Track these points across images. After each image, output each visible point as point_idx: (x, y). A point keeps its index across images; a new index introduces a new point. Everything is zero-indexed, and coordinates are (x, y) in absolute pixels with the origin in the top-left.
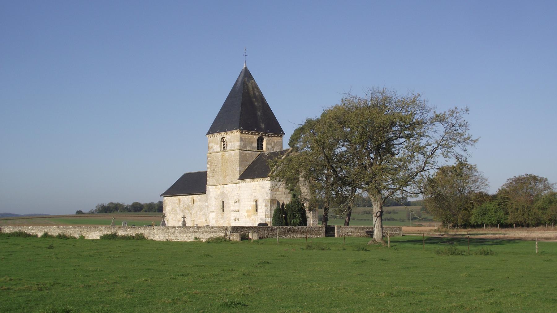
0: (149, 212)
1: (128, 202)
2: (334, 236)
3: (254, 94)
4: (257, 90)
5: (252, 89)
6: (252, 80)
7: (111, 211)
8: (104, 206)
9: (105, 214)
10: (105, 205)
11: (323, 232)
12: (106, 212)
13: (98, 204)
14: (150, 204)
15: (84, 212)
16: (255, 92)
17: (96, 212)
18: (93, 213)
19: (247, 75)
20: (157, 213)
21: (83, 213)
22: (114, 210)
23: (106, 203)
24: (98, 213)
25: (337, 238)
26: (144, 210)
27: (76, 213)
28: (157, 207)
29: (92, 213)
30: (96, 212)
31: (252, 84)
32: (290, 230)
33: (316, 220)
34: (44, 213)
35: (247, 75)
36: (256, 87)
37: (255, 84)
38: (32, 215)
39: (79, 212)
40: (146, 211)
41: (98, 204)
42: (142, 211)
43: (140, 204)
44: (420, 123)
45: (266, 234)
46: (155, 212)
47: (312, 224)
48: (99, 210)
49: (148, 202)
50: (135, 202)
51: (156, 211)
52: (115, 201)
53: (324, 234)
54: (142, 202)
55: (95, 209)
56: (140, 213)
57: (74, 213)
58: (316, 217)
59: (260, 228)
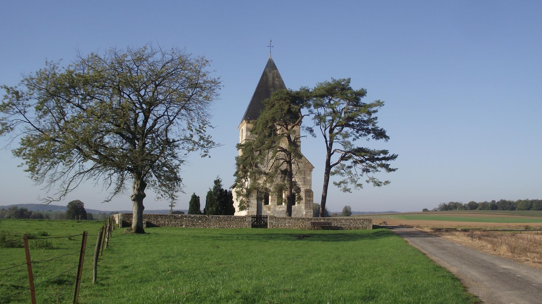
0: (483, 210)
1: (465, 201)
2: (267, 228)
3: (273, 83)
4: (278, 79)
5: (271, 79)
6: (275, 70)
7: (451, 209)
8: (445, 204)
9: (447, 212)
10: (446, 204)
11: (248, 222)
12: (447, 210)
13: (441, 204)
14: (484, 203)
15: (429, 210)
16: (275, 82)
17: (438, 210)
18: (436, 210)
19: (271, 66)
20: (490, 211)
21: (428, 211)
22: (453, 208)
23: (447, 203)
24: (440, 210)
25: (269, 229)
26: (479, 208)
27: (67, 205)
28: (490, 206)
29: (435, 210)
30: (438, 210)
31: (273, 74)
32: (200, 219)
33: (310, 211)
34: (28, 203)
35: (271, 66)
36: (279, 76)
37: (277, 74)
38: (391, 212)
39: (425, 210)
40: (480, 209)
41: (441, 204)
42: (477, 209)
43: (475, 203)
44: (326, 90)
45: (167, 223)
46: (488, 209)
47: (305, 215)
48: (441, 208)
49: (482, 201)
50: (471, 201)
51: (490, 209)
52: (455, 201)
53: (249, 225)
54: (477, 201)
55: (437, 207)
56: (475, 210)
57: (421, 211)
58: (310, 208)
59: (159, 217)
